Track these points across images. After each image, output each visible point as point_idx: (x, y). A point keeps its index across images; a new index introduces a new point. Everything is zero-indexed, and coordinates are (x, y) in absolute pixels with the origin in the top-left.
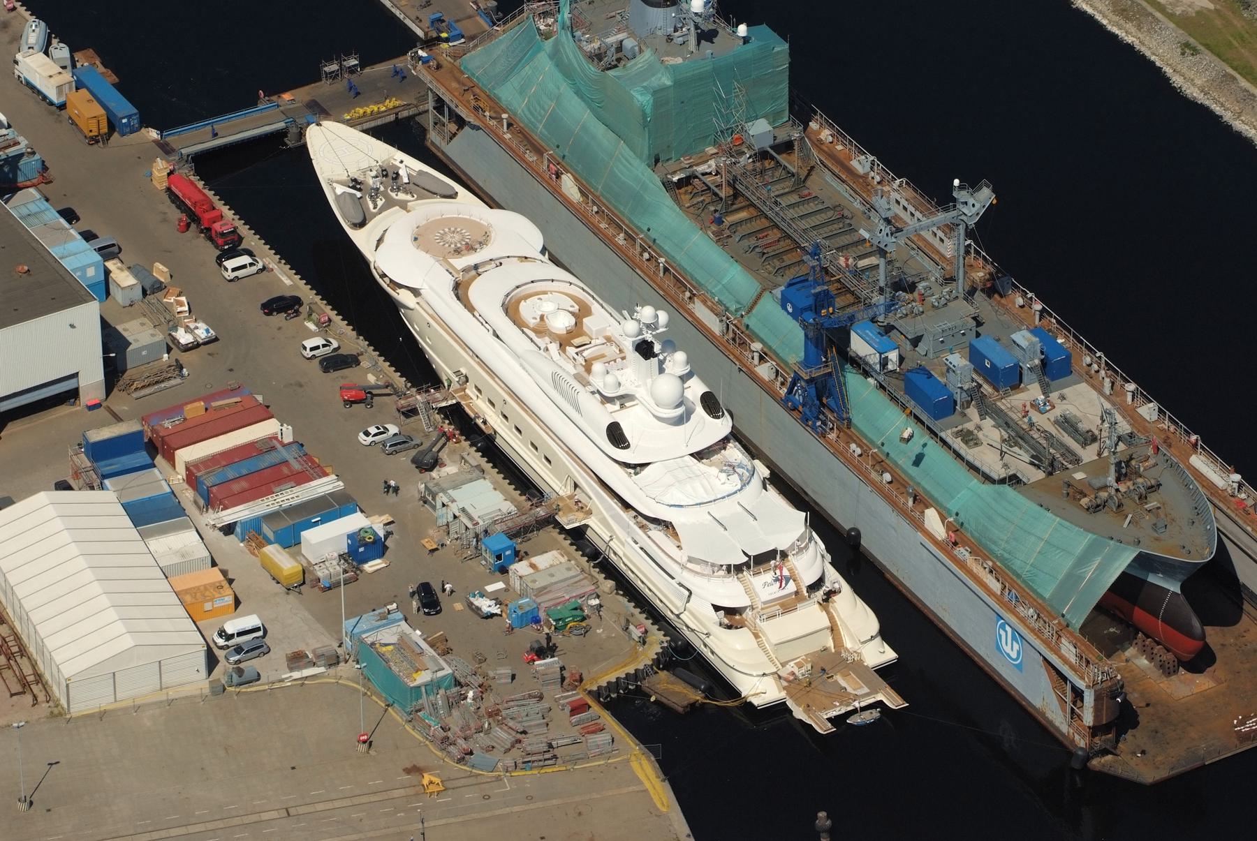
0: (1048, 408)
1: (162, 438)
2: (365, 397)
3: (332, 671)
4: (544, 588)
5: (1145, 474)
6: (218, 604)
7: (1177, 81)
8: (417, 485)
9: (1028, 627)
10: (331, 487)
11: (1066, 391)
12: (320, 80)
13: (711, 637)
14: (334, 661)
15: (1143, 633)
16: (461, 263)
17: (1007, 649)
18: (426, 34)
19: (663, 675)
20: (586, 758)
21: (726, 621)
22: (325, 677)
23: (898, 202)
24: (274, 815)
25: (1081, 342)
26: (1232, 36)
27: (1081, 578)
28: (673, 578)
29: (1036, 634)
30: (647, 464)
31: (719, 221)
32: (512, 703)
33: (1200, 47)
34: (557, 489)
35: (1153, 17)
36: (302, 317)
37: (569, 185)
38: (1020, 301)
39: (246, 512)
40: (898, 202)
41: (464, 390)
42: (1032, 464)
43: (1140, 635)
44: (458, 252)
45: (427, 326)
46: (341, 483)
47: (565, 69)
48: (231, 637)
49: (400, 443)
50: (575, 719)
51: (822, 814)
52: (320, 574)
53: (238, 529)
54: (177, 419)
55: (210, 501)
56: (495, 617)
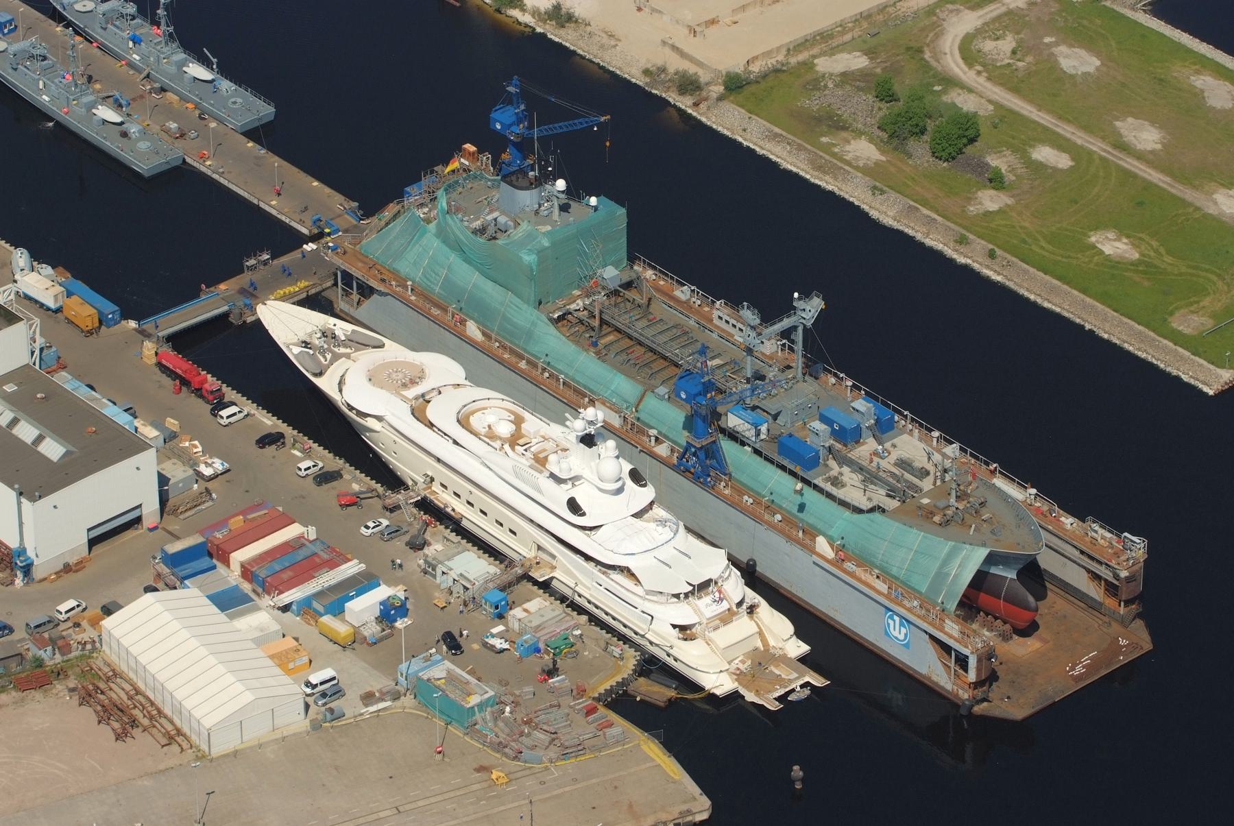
0: (886, 454)
1: (217, 546)
2: (353, 502)
3: (398, 703)
4: (539, 626)
5: (973, 494)
6: (298, 663)
7: (874, 214)
8: (417, 561)
9: (916, 615)
10: (356, 568)
11: (895, 441)
14: (396, 696)
15: (984, 612)
16: (412, 392)
17: (896, 633)
18: (310, 231)
19: (642, 680)
20: (606, 746)
21: (681, 636)
22: (392, 709)
23: (720, 318)
24: (388, 813)
25: (888, 406)
26: (906, 178)
27: (948, 575)
28: (636, 608)
29: (922, 619)
30: (602, 526)
31: (595, 344)
32: (540, 713)
33: (885, 188)
34: (525, 554)
35: (844, 170)
36: (287, 447)
37: (473, 330)
38: (833, 380)
39: (299, 594)
40: (720, 318)
41: (430, 488)
42: (888, 495)
43: (982, 613)
44: (404, 386)
45: (393, 443)
46: (362, 565)
47: (457, 247)
48: (315, 686)
49: (394, 532)
50: (591, 718)
51: (796, 768)
52: (366, 634)
53: (294, 607)
54: (225, 531)
55: (269, 587)
56: (505, 652)
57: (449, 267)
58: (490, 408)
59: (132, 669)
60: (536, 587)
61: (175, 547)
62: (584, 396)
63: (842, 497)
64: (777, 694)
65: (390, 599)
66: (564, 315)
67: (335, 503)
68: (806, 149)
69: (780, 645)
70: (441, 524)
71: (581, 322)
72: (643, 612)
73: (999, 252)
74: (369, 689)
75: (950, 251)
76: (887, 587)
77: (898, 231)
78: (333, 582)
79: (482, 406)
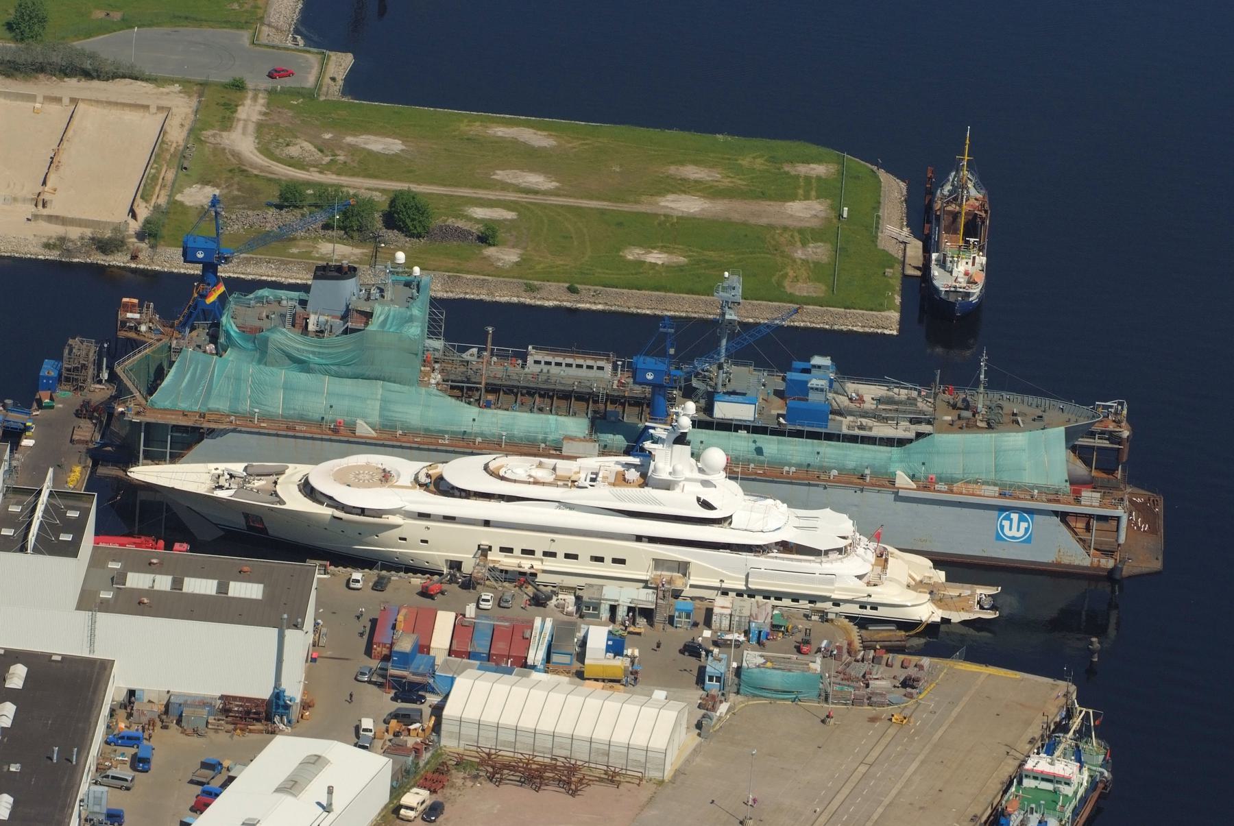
17: (1014, 533)
23: (537, 362)
34: (644, 578)
40: (537, 362)
59: (504, 743)
68: (291, 262)
77: (460, 299)
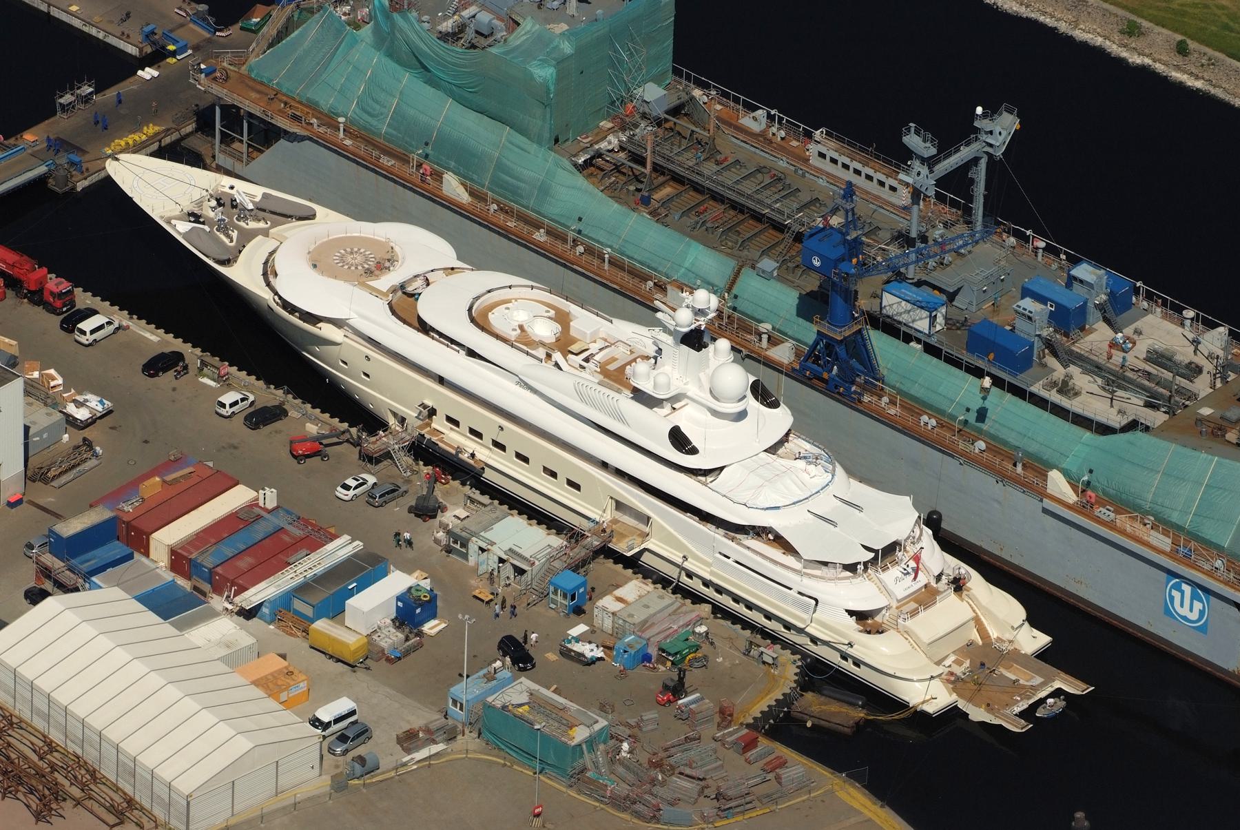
1: (128, 523)
2: (314, 451)
4: (645, 621)
6: (294, 692)
8: (432, 535)
10: (350, 548)
11: (1138, 324)
12: (54, 114)
13: (855, 646)
14: (451, 736)
16: (386, 282)
17: (1184, 611)
18: (141, 50)
19: (809, 696)
22: (448, 754)
23: (822, 155)
28: (790, 589)
30: (722, 469)
31: (646, 201)
32: (673, 750)
37: (453, 187)
40: (822, 155)
41: (429, 425)
44: (369, 273)
46: (357, 543)
47: (419, 64)
48: (328, 725)
53: (265, 610)
56: (598, 663)
57: (401, 93)
58: (516, 300)
59: (39, 713)
60: (621, 566)
61: (71, 527)
62: (645, 278)
63: (1079, 411)
64: (1017, 710)
65: (413, 591)
66: (592, 158)
67: (285, 453)
69: (1007, 636)
70: (454, 479)
71: (618, 168)
72: (800, 593)
73: (1192, 45)
74: (406, 727)
75: (1115, 47)
76: (1169, 541)
77: (1028, 20)
78: (319, 570)
79: (502, 298)
